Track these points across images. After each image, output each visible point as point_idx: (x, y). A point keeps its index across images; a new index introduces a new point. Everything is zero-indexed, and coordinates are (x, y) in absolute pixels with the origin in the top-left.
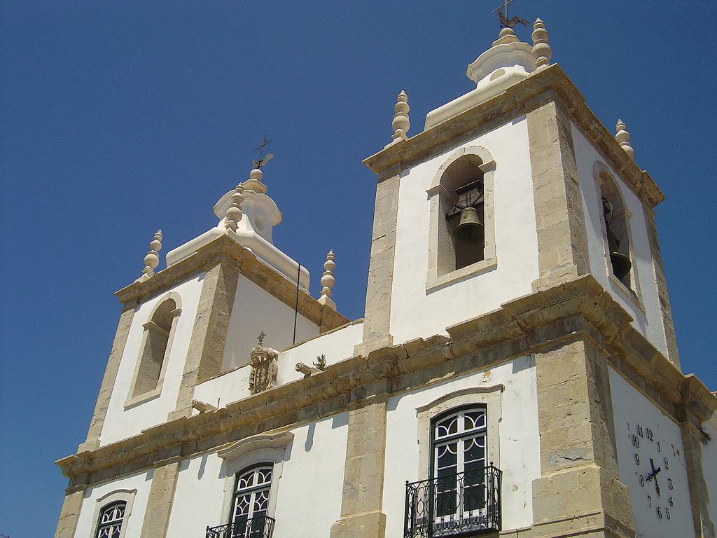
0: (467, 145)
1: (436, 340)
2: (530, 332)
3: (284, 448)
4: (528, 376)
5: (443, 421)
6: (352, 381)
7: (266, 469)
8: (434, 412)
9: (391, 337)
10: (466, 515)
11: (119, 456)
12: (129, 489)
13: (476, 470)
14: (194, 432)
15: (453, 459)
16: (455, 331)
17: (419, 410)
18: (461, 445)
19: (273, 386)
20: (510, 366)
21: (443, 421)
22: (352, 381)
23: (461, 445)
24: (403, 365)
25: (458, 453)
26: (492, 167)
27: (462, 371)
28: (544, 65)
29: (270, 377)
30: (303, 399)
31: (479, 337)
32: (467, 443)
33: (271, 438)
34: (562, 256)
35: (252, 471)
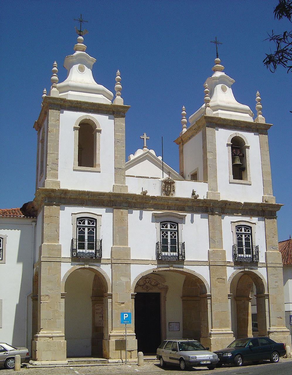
0: (90, 114)
1: (239, 203)
2: (263, 211)
3: (182, 219)
4: (262, 223)
5: (81, 220)
6: (211, 205)
7: (174, 224)
8: (237, 224)
9: (58, 183)
10: (88, 251)
11: (87, 196)
12: (98, 214)
13: (173, 241)
14: (136, 200)
15: (242, 239)
16: (246, 204)
17: (232, 222)
18: (86, 229)
19: (171, 196)
20: (104, 210)
21: (81, 220)
22: (211, 205)
23: (86, 229)
24: (227, 206)
25: (85, 231)
26: (75, 129)
27: (243, 215)
28: (248, 115)
29: (172, 189)
30: (190, 204)
31: (251, 207)
32: (89, 229)
33: (179, 215)
34: (270, 191)
35: (84, 219)
